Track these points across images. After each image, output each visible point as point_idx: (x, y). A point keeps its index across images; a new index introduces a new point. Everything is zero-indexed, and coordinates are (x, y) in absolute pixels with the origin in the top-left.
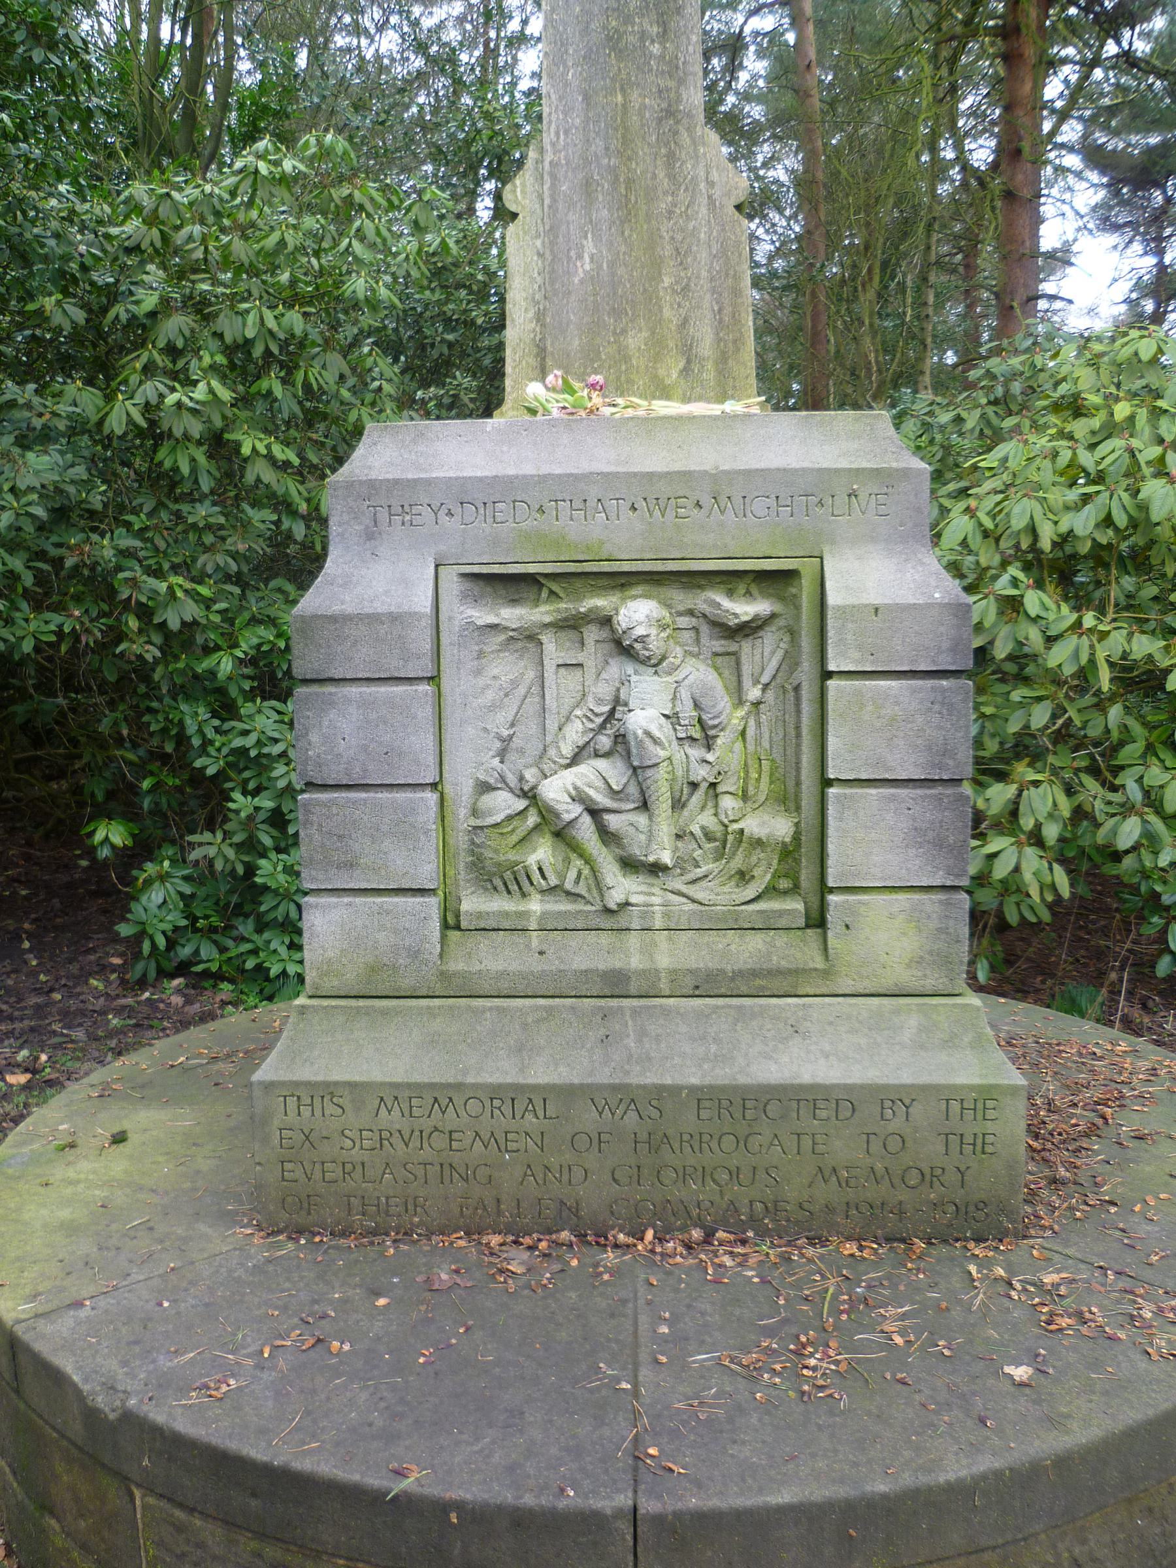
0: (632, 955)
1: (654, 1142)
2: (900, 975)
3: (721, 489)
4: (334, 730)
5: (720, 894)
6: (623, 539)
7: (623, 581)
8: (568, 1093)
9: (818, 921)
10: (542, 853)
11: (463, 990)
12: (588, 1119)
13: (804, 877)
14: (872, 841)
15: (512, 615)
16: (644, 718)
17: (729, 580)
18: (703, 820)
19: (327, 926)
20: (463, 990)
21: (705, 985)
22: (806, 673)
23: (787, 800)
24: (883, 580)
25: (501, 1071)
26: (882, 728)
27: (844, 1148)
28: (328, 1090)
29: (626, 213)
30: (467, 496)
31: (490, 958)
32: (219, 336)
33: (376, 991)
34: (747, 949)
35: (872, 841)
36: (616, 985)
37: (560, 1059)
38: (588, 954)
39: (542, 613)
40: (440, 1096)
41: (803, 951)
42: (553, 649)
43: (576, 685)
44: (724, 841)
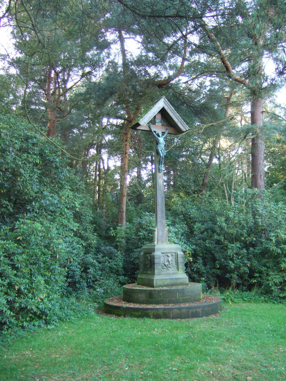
4: (156, 261)
6: (167, 251)
7: (168, 253)
9: (178, 270)
10: (165, 267)
15: (163, 255)
19: (156, 271)
28: (178, 278)
34: (175, 272)
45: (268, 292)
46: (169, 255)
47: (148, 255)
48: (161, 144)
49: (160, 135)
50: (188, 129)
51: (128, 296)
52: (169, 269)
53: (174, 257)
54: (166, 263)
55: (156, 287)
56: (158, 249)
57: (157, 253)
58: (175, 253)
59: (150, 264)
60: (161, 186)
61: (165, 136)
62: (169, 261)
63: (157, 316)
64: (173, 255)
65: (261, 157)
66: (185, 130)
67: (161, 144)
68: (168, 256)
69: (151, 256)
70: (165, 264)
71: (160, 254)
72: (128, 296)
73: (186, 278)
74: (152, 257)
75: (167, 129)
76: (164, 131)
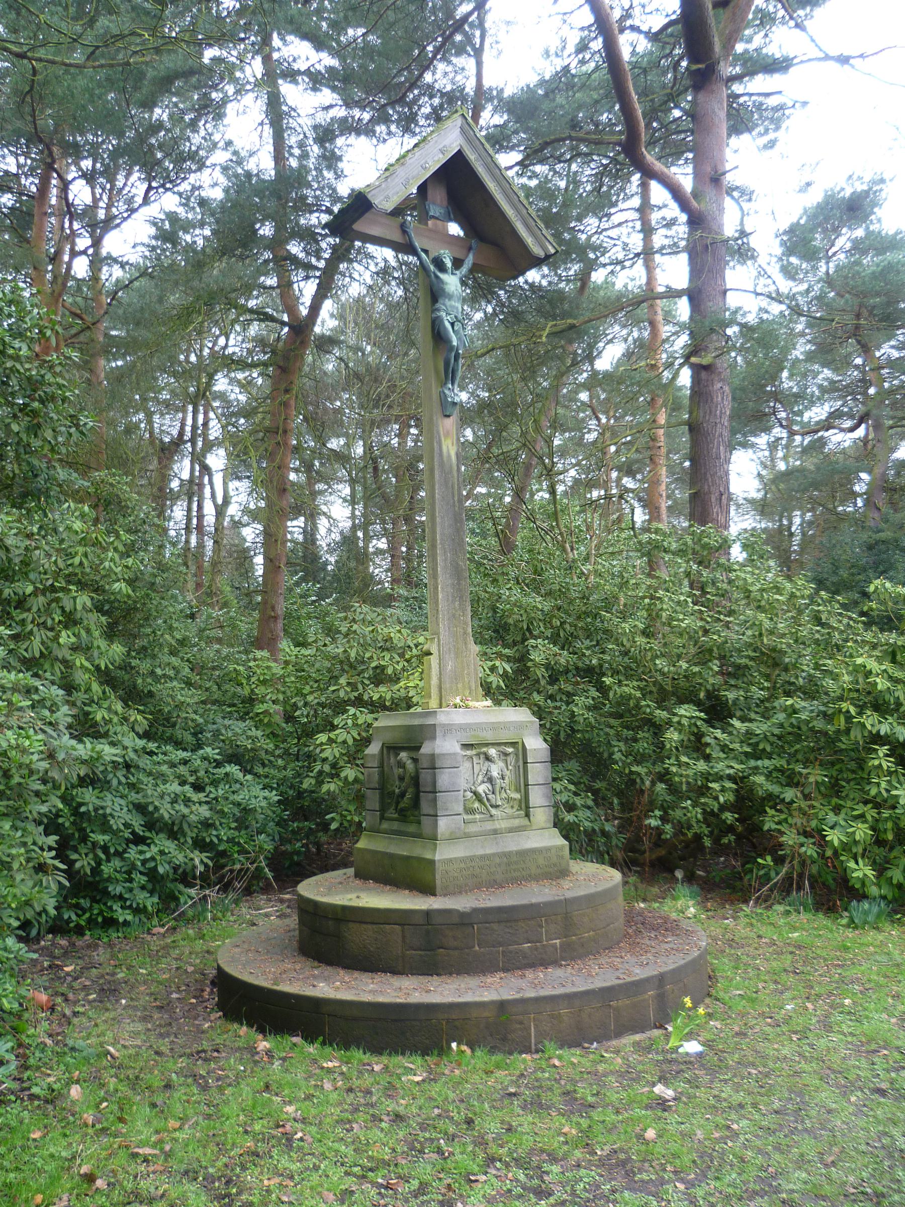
0: (497, 825)
1: (508, 864)
2: (543, 825)
3: (505, 726)
4: (444, 779)
5: (509, 811)
6: (489, 736)
7: (487, 745)
8: (494, 855)
9: (527, 815)
10: (476, 805)
11: (468, 836)
12: (498, 860)
13: (526, 807)
14: (537, 797)
15: (469, 753)
16: (495, 773)
17: (505, 744)
18: (504, 795)
19: (443, 824)
20: (468, 836)
21: (511, 830)
22: (521, 763)
23: (518, 790)
24: (536, 745)
25: (481, 852)
26: (538, 772)
27: (541, 861)
28: (451, 860)
29: (457, 657)
30: (463, 728)
31: (473, 828)
32: (62, 608)
33: (453, 838)
34: (517, 822)
35: (537, 797)
36: (495, 832)
37: (490, 849)
38: (489, 826)
39: (474, 752)
40: (472, 859)
41: (525, 821)
42: (475, 760)
43: (481, 766)
44: (509, 800)
45: (832, 893)
46: (492, 752)
47: (403, 755)
48: (450, 297)
49: (449, 264)
50: (553, 251)
51: (325, 937)
52: (493, 811)
53: (511, 759)
54: (482, 789)
55: (459, 890)
56: (449, 729)
57: (446, 746)
58: (513, 744)
59: (407, 794)
60: (451, 471)
61: (464, 270)
62: (490, 780)
63: (499, 1030)
64: (506, 754)
65: (721, 435)
66: (542, 254)
67: (450, 297)
68: (488, 758)
69: (415, 760)
70: (475, 793)
71: (457, 748)
72: (325, 937)
73: (561, 848)
74: (424, 763)
75: (470, 249)
76: (459, 256)
